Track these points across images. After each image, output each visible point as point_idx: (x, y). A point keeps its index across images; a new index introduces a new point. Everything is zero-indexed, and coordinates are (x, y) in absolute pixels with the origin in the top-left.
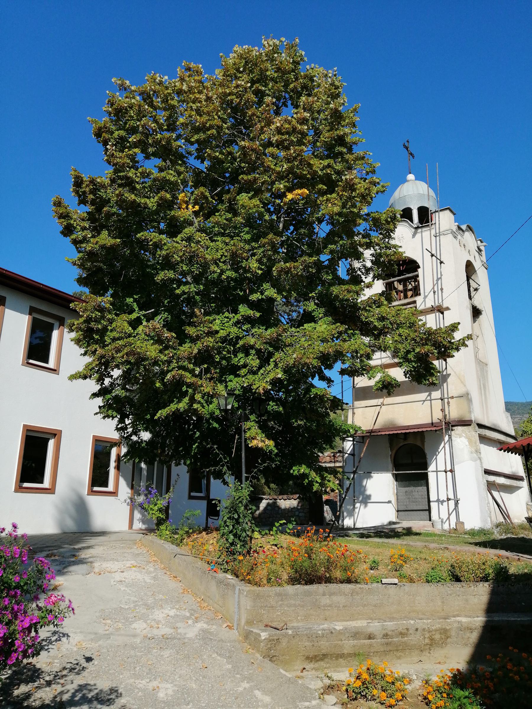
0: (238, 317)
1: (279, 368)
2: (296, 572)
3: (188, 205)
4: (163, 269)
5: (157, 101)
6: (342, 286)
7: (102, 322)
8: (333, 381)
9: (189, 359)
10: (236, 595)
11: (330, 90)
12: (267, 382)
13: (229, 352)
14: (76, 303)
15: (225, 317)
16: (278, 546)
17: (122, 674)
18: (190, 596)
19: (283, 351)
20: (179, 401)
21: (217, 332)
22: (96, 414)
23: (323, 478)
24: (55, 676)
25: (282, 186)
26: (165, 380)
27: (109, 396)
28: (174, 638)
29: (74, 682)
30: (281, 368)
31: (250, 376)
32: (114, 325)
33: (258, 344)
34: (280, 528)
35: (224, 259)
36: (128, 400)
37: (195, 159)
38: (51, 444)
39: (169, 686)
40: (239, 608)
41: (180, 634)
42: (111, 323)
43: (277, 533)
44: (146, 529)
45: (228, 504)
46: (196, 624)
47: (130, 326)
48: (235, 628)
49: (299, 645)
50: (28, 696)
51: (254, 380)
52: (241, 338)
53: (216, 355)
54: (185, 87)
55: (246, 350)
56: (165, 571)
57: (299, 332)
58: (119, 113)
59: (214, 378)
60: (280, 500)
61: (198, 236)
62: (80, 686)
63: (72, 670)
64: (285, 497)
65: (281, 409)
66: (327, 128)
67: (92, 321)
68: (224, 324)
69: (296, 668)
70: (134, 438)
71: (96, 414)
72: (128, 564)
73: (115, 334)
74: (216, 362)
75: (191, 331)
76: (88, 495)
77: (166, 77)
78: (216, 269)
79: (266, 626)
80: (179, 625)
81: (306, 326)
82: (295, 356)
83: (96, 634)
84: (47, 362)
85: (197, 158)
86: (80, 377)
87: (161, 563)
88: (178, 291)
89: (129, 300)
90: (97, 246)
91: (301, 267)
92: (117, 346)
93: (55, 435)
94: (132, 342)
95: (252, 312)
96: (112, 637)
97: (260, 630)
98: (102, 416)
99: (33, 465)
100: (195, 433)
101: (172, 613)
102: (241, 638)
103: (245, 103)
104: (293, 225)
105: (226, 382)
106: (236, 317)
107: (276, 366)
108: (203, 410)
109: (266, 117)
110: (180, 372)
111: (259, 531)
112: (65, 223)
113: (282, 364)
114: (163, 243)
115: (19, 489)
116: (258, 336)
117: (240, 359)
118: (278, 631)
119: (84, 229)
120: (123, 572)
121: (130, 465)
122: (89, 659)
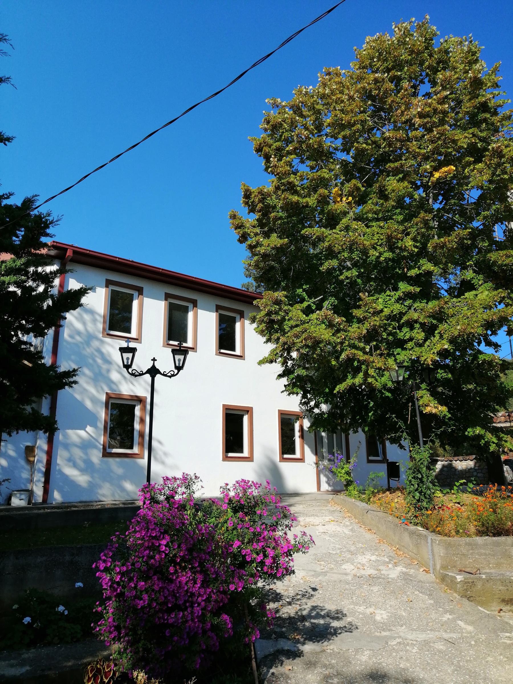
0: (399, 293)
1: (445, 339)
2: (483, 525)
3: (342, 198)
4: (327, 259)
5: (305, 111)
6: (500, 252)
7: (280, 313)
8: (500, 346)
9: (359, 339)
10: (429, 544)
11: (466, 58)
12: (434, 353)
13: (394, 328)
14: (258, 300)
15: (387, 296)
16: (461, 504)
17: (343, 601)
18: (386, 545)
19: (447, 323)
20: (354, 377)
21: (382, 311)
22: (283, 392)
23: (500, 439)
24: (293, 599)
25: (428, 167)
26: (340, 360)
27: (292, 376)
28: (379, 578)
29: (308, 604)
30: (447, 339)
31: (417, 349)
32: (290, 315)
33: (422, 318)
34: (461, 487)
35: (380, 242)
36: (309, 379)
37: (341, 152)
38: (246, 418)
39: (383, 612)
40: (433, 555)
41: (384, 575)
42: (288, 314)
43: (458, 492)
44: (332, 491)
45: (411, 466)
46: (396, 568)
47: (304, 314)
48: (431, 571)
49: (494, 588)
50: (277, 611)
51: (421, 352)
52: (404, 314)
53: (383, 332)
54: (327, 91)
55: (410, 324)
56: (360, 525)
57: (460, 301)
58: (275, 128)
59: (385, 354)
60: (456, 461)
61: (354, 225)
62: (312, 606)
63: (304, 596)
64: (461, 458)
65: (450, 376)
66: (468, 97)
67: (273, 314)
68: (386, 303)
69: (493, 608)
70: (316, 411)
71: (283, 392)
72: (327, 519)
73: (292, 323)
74: (384, 339)
75: (358, 313)
76: (280, 461)
77: (311, 87)
78: (375, 253)
79: (461, 571)
80: (381, 567)
81: (467, 295)
82: (459, 327)
83: (315, 571)
84: (234, 349)
85: (343, 151)
86: (267, 362)
87: (355, 518)
88: (342, 277)
89: (299, 291)
90: (269, 248)
91: (455, 240)
92: (296, 332)
93: (248, 411)
94: (308, 327)
95: (412, 288)
96: (328, 574)
97: (455, 573)
98: (288, 393)
99: (231, 438)
100: (369, 403)
101: (373, 558)
102: (438, 581)
103: (384, 93)
104: (442, 195)
105: (395, 356)
106: (397, 294)
107: (441, 337)
108: (377, 383)
109: (406, 101)
110: (353, 351)
111: (440, 490)
112: (241, 232)
113: (447, 335)
114: (325, 235)
115: (226, 458)
116: (421, 311)
117: (405, 333)
118: (472, 576)
119: (256, 234)
120: (324, 525)
121: (312, 435)
122: (314, 589)
